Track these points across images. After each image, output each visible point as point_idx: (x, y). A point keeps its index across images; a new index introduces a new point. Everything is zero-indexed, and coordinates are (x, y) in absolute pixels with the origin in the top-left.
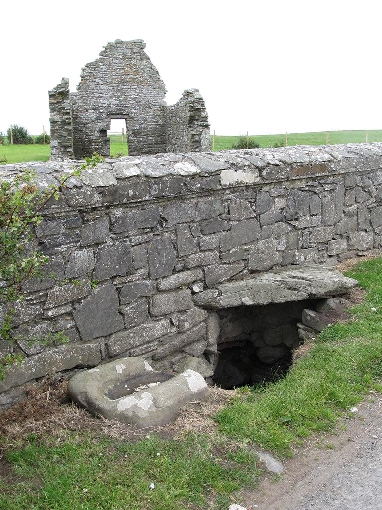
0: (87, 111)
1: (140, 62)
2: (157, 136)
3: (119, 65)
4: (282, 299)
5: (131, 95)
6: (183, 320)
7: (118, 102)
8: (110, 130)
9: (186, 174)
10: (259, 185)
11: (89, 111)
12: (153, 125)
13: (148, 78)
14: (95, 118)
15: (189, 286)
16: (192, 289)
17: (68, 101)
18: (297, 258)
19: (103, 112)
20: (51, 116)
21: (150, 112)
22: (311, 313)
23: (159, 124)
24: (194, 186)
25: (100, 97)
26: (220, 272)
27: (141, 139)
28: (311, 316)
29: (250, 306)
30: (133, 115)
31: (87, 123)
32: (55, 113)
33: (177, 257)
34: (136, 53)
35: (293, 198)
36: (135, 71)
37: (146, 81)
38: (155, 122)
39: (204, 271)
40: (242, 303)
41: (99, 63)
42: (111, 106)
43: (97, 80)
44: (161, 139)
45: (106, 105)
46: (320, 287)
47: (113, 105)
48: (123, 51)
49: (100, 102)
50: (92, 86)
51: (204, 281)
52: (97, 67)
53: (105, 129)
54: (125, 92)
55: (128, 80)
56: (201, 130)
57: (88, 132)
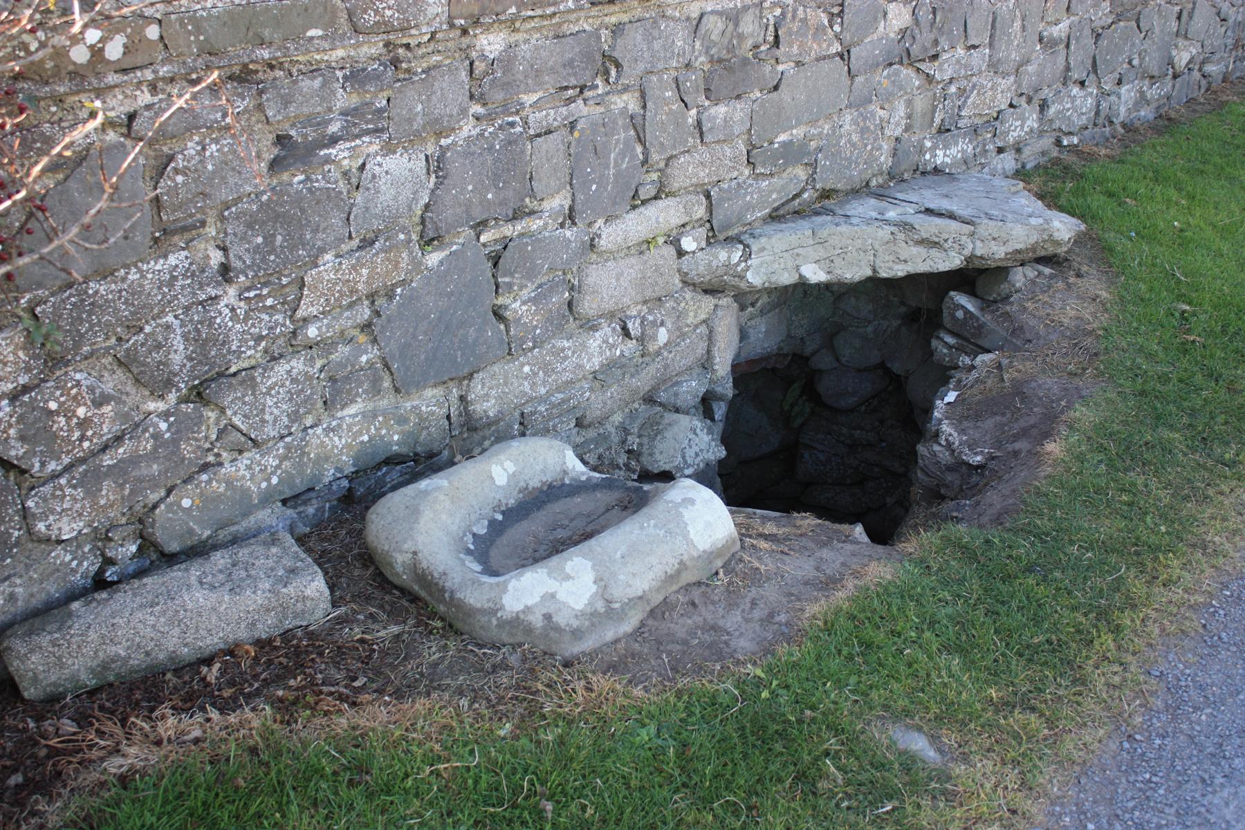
6: (654, 323)
26: (748, 198)
46: (994, 239)
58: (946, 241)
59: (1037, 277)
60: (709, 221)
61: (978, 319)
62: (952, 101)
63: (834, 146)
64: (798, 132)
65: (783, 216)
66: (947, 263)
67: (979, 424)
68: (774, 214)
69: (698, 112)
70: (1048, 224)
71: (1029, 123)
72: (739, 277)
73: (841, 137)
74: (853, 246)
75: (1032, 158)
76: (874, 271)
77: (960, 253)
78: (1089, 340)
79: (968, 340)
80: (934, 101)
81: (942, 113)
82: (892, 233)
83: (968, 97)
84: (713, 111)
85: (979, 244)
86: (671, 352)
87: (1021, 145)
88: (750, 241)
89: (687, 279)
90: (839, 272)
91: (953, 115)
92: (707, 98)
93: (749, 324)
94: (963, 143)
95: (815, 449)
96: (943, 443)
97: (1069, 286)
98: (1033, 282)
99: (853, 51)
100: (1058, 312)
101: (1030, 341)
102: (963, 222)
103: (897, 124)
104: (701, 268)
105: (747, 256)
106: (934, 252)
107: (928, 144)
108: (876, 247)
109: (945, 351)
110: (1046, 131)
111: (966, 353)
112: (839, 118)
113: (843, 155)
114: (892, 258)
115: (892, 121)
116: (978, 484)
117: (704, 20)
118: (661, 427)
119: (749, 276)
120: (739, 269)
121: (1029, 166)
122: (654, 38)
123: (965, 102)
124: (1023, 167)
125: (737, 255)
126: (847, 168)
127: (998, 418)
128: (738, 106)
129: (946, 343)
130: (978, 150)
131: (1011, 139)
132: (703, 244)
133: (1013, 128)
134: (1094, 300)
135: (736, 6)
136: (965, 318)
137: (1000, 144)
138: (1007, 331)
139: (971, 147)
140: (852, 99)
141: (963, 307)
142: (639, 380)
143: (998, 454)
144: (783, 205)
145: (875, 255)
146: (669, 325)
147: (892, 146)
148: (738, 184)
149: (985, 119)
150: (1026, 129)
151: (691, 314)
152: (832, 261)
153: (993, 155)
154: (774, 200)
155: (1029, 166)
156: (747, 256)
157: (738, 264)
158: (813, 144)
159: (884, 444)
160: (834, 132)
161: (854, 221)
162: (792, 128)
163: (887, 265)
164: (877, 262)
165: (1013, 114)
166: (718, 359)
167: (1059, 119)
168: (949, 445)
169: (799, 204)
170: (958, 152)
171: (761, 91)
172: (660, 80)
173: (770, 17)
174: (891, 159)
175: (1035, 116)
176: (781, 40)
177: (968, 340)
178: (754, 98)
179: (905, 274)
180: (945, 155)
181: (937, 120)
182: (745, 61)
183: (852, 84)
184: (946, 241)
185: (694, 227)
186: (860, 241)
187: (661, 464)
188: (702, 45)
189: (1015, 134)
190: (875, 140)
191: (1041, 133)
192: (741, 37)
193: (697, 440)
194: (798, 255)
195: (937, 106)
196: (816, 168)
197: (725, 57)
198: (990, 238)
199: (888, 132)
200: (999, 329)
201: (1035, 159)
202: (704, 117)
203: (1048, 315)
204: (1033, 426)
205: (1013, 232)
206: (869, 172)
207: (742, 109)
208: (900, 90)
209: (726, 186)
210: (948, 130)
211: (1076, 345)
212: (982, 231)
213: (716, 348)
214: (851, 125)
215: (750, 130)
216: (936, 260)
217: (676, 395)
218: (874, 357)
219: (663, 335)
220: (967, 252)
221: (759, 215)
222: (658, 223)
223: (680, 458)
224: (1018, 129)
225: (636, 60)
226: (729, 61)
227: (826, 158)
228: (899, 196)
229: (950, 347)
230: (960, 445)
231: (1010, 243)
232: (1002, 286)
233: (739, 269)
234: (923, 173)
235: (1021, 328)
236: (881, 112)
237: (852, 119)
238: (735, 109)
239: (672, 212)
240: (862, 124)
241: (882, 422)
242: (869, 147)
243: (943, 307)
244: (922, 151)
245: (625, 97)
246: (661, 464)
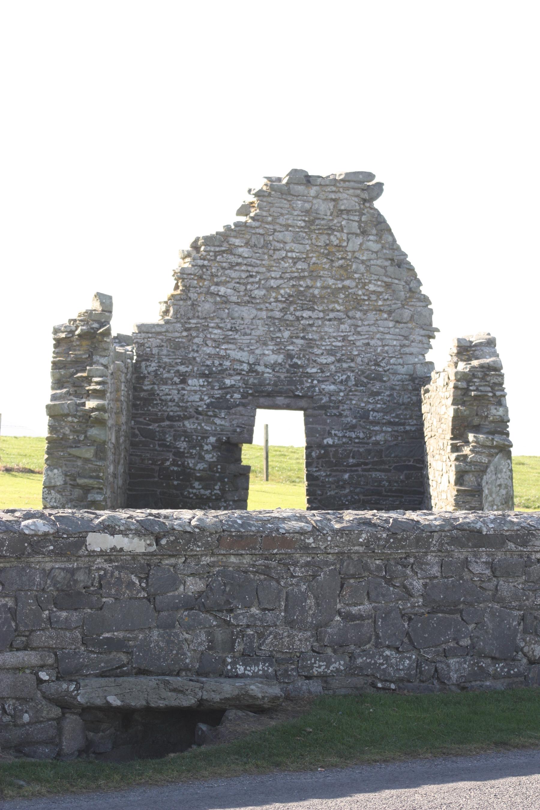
0: (183, 381)
1: (359, 240)
2: (396, 468)
3: (294, 246)
4: (162, 702)
5: (322, 339)
6: (21, 710)
7: (280, 358)
8: (250, 441)
9: (33, 532)
10: (155, 556)
11: (190, 382)
12: (386, 432)
13: (379, 289)
14: (208, 405)
15: (35, 670)
16: (36, 674)
17: (104, 361)
18: (229, 667)
19: (232, 386)
20: (54, 398)
21: (378, 393)
22: (204, 727)
23: (406, 432)
24: (44, 547)
25: (227, 340)
26: (81, 660)
27: (346, 476)
28: (202, 730)
29: (117, 708)
30: (325, 399)
31: (181, 419)
32: (64, 390)
33: (16, 630)
34: (348, 212)
35: (222, 580)
36: (341, 266)
37: (373, 297)
38: (390, 423)
39: (56, 655)
40: (108, 702)
41: (233, 240)
42: (260, 369)
43: (222, 290)
44: (408, 477)
45: (245, 367)
46: (214, 691)
47: (266, 366)
48: (307, 206)
49: (227, 357)
50: (206, 307)
51: (57, 668)
52: (224, 252)
53: (234, 439)
54: (304, 330)
55: (316, 292)
56: (485, 460)
57: (182, 445)
58: (187, 690)
64: (120, 635)
66: (188, 702)
72: (73, 698)
73: (151, 642)
74: (136, 689)
76: (148, 703)
77: (195, 697)
82: (157, 684)
83: (266, 639)
85: (205, 693)
90: (128, 701)
92: (56, 607)
99: (157, 598)
104: (53, 691)
105: (77, 689)
106: (180, 696)
108: (148, 690)
114: (157, 696)
117: (53, 571)
119: (79, 698)
120: (73, 694)
122: (22, 575)
123: (264, 641)
125: (72, 687)
128: (75, 614)
132: (54, 678)
135: (73, 566)
142: (10, 735)
144: (109, 670)
145: (148, 695)
151: (45, 712)
152: (124, 696)
156: (77, 689)
164: (149, 698)
166: (65, 743)
172: (26, 594)
173: (96, 574)
176: (103, 586)
182: (79, 593)
183: (158, 615)
184: (187, 690)
186: (139, 687)
188: (51, 582)
192: (76, 581)
194: (106, 690)
195: (235, 639)
197: (66, 589)
205: (225, 688)
207: (77, 616)
209: (67, 651)
214: (158, 637)
219: (26, 718)
222: (23, 660)
225: (13, 584)
231: (223, 694)
233: (73, 694)
238: (73, 615)
239: (33, 657)
242: (174, 652)
245: (7, 599)
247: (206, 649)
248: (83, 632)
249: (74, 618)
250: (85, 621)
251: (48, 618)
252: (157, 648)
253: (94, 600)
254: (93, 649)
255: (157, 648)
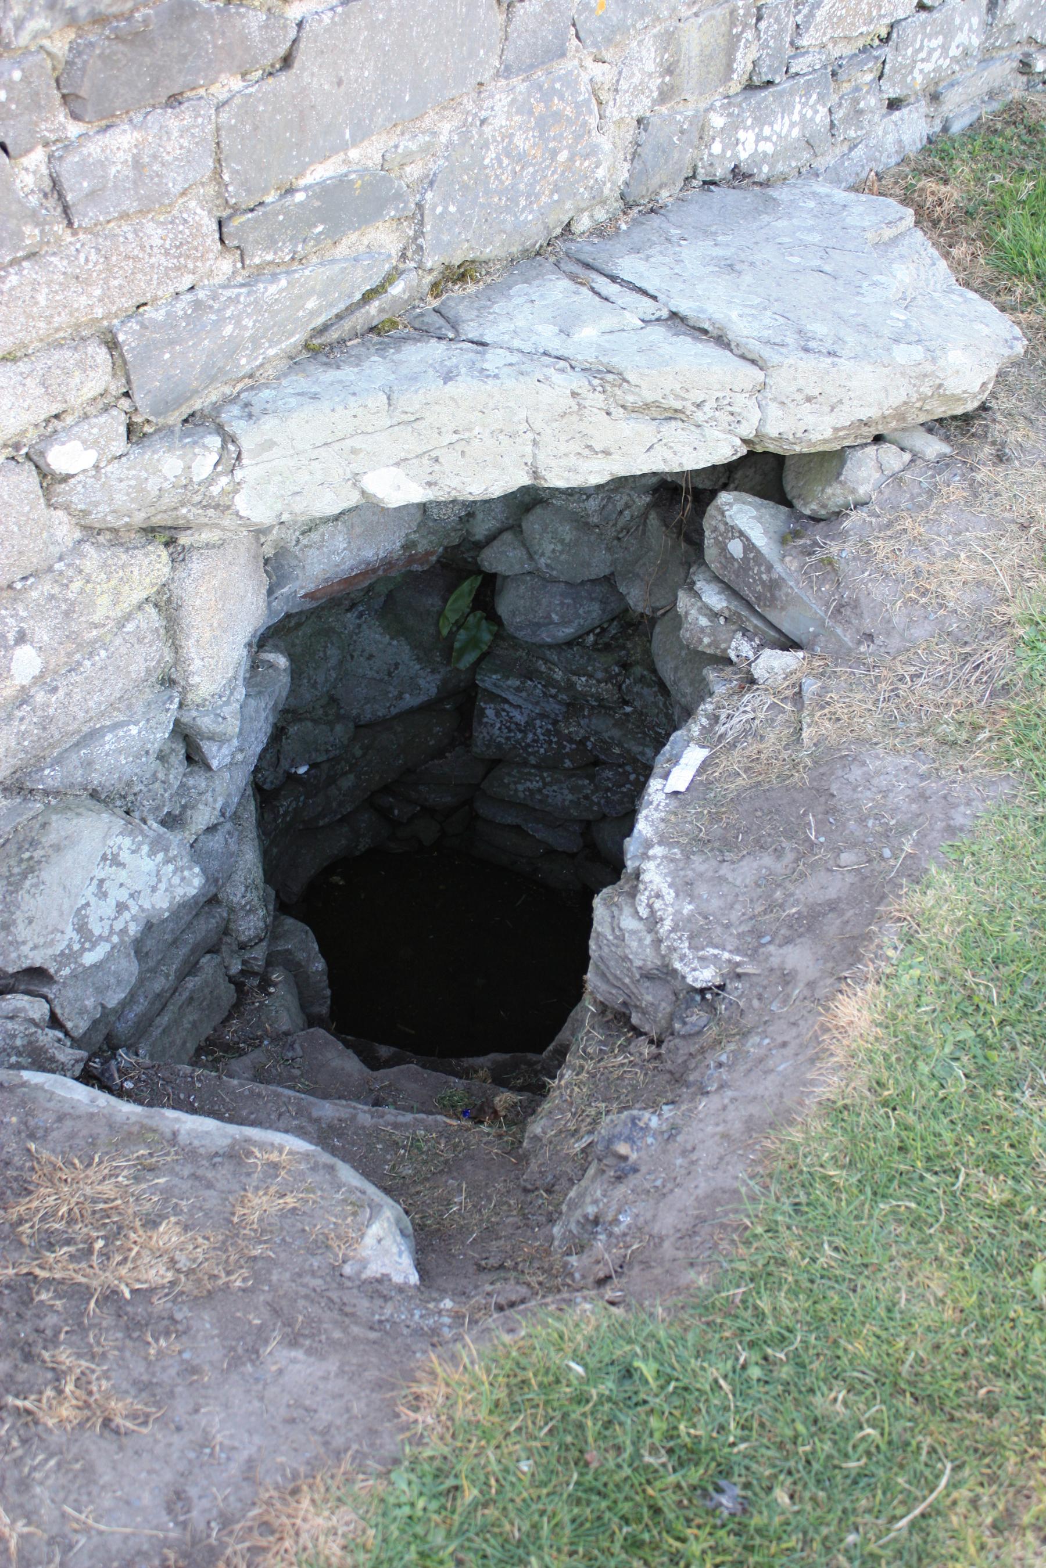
26: (228, 330)
46: (809, 399)
59: (906, 468)
60: (127, 394)
61: (770, 568)
62: (778, 20)
63: (466, 169)
65: (342, 342)
67: (725, 870)
68: (317, 342)
69: (50, 157)
70: (934, 360)
71: (961, 38)
73: (486, 145)
75: (965, 107)
78: (996, 649)
79: (749, 605)
80: (733, 24)
81: (754, 48)
82: (574, 394)
84: (93, 149)
85: (774, 410)
86: (55, 690)
87: (942, 84)
88: (237, 427)
89: (93, 519)
90: (455, 482)
91: (780, 49)
92: (75, 116)
93: (304, 541)
94: (804, 105)
95: (506, 701)
96: (644, 912)
97: (974, 488)
98: (897, 479)
100: (938, 566)
101: (870, 637)
102: (743, 357)
103: (638, 90)
104: (120, 499)
107: (718, 121)
108: (538, 426)
109: (704, 621)
110: (1001, 48)
111: (745, 632)
112: (478, 102)
113: (493, 185)
114: (576, 446)
115: (623, 85)
116: (699, 1033)
118: (38, 854)
119: (241, 503)
120: (215, 490)
121: (956, 128)
123: (811, 15)
124: (945, 129)
126: (507, 209)
127: (767, 860)
129: (706, 606)
130: (839, 114)
131: (919, 78)
133: (923, 55)
134: (1024, 527)
136: (745, 558)
137: (893, 93)
138: (827, 605)
139: (823, 111)
140: (509, 56)
141: (742, 534)
143: (749, 969)
144: (339, 317)
145: (535, 443)
146: (42, 634)
147: (629, 137)
148: (197, 305)
149: (860, 44)
150: (954, 52)
151: (104, 601)
152: (437, 460)
153: (877, 118)
154: (313, 314)
155: (956, 128)
157: (210, 481)
158: (414, 171)
159: (628, 709)
160: (465, 137)
161: (494, 360)
162: (345, 147)
163: (564, 462)
164: (541, 457)
165: (924, 25)
167: (1030, 19)
168: (653, 921)
169: (381, 310)
170: (793, 125)
171: (244, 75)
174: (627, 166)
175: (975, 21)
177: (749, 605)
178: (223, 96)
179: (608, 478)
180: (760, 138)
181: (743, 63)
183: (509, 20)
185: (86, 416)
187: (25, 949)
189: (928, 67)
190: (578, 138)
191: (987, 56)
193: (122, 875)
194: (354, 451)
195: (739, 37)
196: (422, 223)
198: (799, 397)
199: (612, 112)
200: (809, 597)
201: (973, 109)
202: (66, 170)
203: (917, 573)
204: (833, 906)
206: (568, 205)
207: (183, 131)
208: (642, 16)
210: (770, 83)
211: (966, 657)
212: (781, 382)
213: (191, 642)
214: (509, 117)
215: (218, 173)
216: (677, 447)
217: (88, 764)
218: (599, 564)
220: (747, 430)
221: (272, 352)
223: (70, 933)
224: (936, 54)
226: (129, 18)
227: (447, 198)
228: (628, 267)
229: (714, 615)
230: (673, 930)
231: (846, 408)
232: (829, 491)
233: (215, 490)
234: (709, 183)
235: (855, 604)
236: (597, 70)
237: (514, 101)
240: (540, 108)
241: (625, 666)
242: (563, 156)
243: (706, 525)
244: (702, 134)
246: (25, 949)
247: (655, 102)
248: (219, 195)
249: (173, 148)
250: (225, 143)
251: (47, 185)
252: (506, 162)
253: (254, 25)
254: (269, 257)
255: (506, 162)
